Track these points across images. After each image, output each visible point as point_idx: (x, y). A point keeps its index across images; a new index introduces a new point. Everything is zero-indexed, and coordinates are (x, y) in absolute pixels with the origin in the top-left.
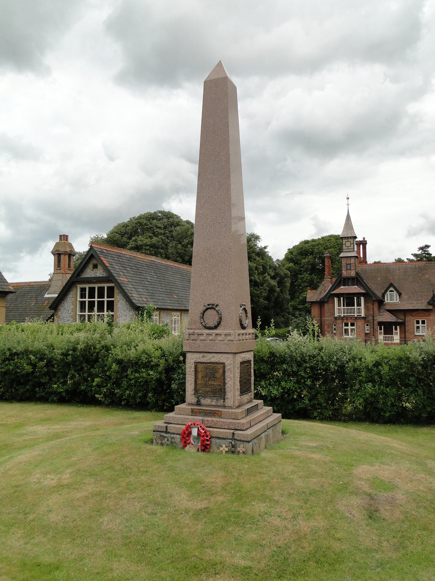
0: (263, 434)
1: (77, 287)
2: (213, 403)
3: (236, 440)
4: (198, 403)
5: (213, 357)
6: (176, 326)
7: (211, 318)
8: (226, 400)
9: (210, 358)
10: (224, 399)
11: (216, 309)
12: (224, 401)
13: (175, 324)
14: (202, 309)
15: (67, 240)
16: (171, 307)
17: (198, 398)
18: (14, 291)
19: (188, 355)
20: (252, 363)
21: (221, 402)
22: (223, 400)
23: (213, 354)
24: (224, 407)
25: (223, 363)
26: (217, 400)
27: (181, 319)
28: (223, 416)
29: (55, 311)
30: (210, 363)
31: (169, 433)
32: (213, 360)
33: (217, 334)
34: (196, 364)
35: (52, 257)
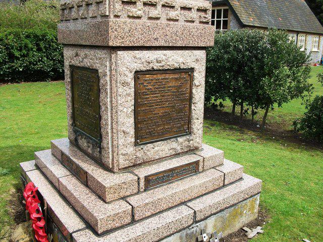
2: (90, 151)
12: (100, 152)
20: (200, 78)
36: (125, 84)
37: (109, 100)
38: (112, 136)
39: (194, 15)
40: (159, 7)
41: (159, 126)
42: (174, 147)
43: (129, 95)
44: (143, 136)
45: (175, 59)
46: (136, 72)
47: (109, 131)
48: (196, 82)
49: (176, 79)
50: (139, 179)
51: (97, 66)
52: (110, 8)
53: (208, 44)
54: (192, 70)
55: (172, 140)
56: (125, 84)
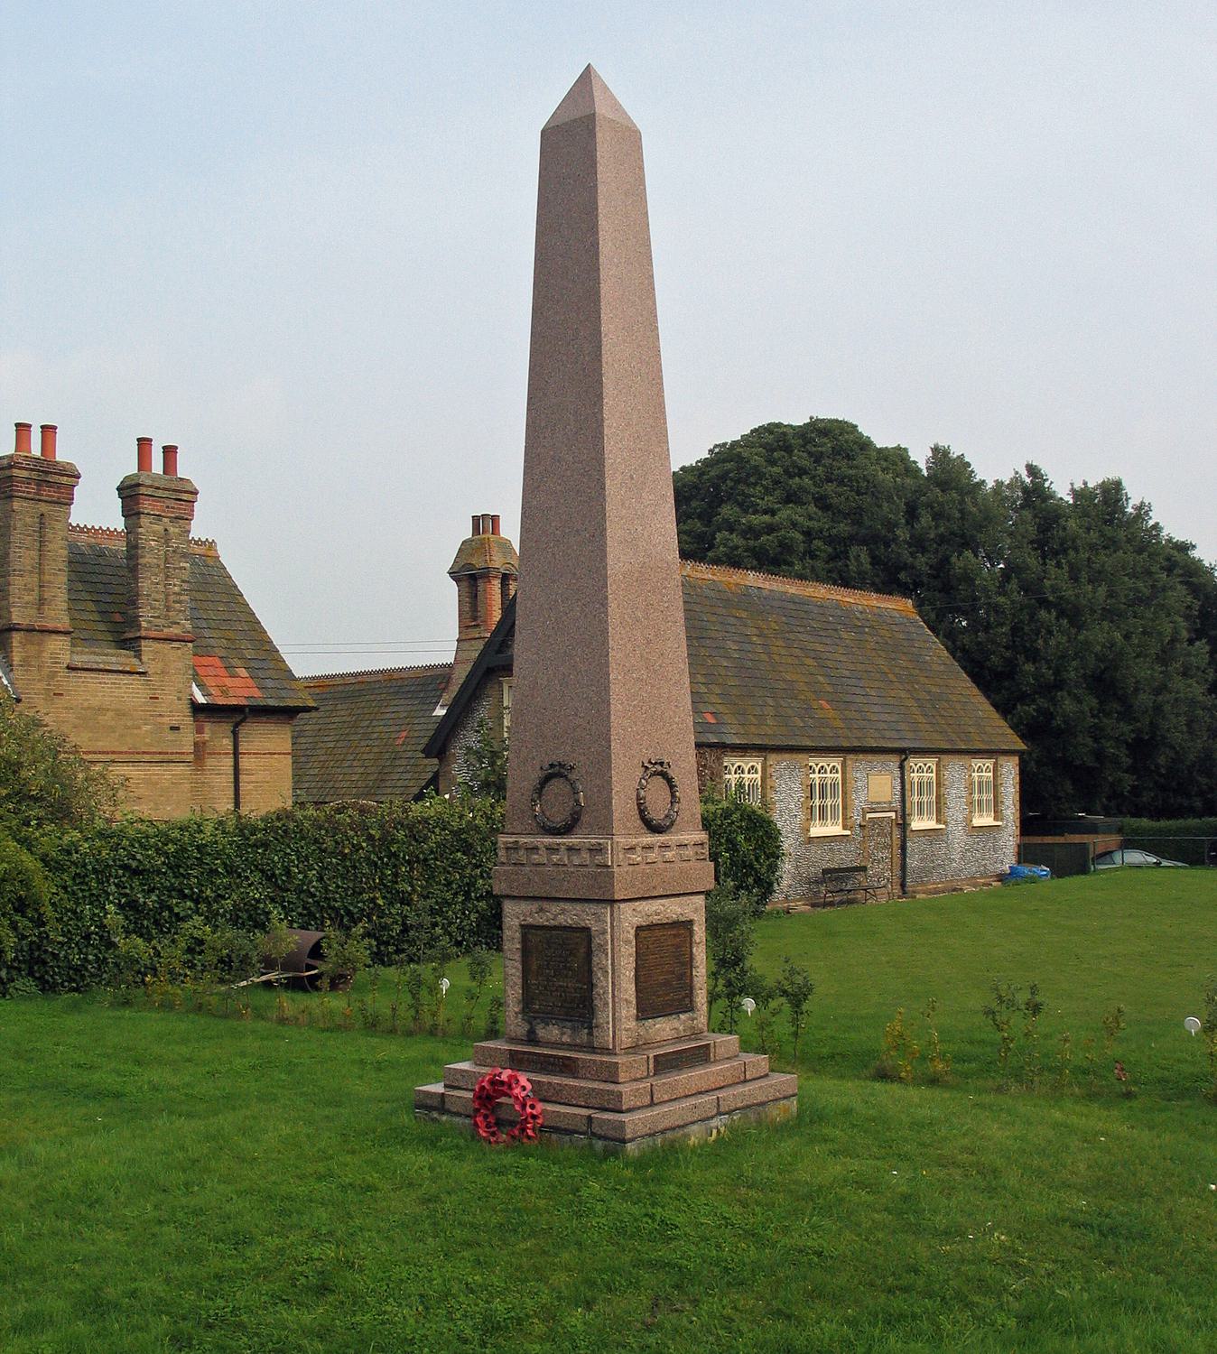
0: (695, 1127)
1: (500, 684)
2: (566, 1039)
3: (594, 1134)
4: (532, 1039)
5: (563, 911)
6: (829, 802)
7: (556, 805)
8: (595, 1030)
9: (556, 916)
10: (590, 1028)
11: (569, 776)
12: (590, 1034)
13: (920, 794)
14: (535, 776)
15: (495, 530)
16: (809, 743)
17: (531, 1024)
18: (312, 704)
19: (508, 907)
20: (700, 933)
21: (583, 1036)
22: (586, 1031)
23: (562, 905)
24: (592, 1049)
25: (587, 930)
26: (574, 1029)
27: (844, 779)
28: (582, 1072)
29: (441, 760)
30: (555, 928)
31: (448, 1112)
32: (562, 920)
33: (570, 849)
34: (526, 929)
35: (452, 588)
36: (627, 942)
37: (610, 962)
38: (614, 1006)
39: (689, 852)
40: (656, 849)
41: (659, 996)
42: (676, 1026)
43: (630, 955)
44: (646, 1010)
45: (672, 909)
46: (637, 927)
47: (610, 1001)
48: (697, 938)
49: (674, 935)
50: (648, 1058)
51: (589, 922)
52: (612, 857)
53: (707, 888)
54: (691, 922)
55: (674, 1016)
56: (627, 942)
